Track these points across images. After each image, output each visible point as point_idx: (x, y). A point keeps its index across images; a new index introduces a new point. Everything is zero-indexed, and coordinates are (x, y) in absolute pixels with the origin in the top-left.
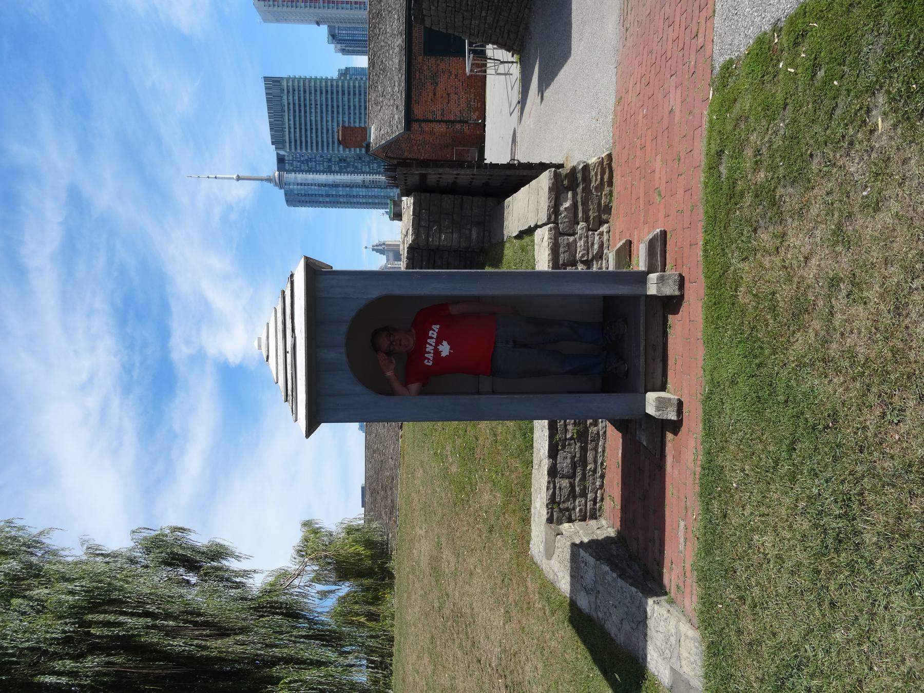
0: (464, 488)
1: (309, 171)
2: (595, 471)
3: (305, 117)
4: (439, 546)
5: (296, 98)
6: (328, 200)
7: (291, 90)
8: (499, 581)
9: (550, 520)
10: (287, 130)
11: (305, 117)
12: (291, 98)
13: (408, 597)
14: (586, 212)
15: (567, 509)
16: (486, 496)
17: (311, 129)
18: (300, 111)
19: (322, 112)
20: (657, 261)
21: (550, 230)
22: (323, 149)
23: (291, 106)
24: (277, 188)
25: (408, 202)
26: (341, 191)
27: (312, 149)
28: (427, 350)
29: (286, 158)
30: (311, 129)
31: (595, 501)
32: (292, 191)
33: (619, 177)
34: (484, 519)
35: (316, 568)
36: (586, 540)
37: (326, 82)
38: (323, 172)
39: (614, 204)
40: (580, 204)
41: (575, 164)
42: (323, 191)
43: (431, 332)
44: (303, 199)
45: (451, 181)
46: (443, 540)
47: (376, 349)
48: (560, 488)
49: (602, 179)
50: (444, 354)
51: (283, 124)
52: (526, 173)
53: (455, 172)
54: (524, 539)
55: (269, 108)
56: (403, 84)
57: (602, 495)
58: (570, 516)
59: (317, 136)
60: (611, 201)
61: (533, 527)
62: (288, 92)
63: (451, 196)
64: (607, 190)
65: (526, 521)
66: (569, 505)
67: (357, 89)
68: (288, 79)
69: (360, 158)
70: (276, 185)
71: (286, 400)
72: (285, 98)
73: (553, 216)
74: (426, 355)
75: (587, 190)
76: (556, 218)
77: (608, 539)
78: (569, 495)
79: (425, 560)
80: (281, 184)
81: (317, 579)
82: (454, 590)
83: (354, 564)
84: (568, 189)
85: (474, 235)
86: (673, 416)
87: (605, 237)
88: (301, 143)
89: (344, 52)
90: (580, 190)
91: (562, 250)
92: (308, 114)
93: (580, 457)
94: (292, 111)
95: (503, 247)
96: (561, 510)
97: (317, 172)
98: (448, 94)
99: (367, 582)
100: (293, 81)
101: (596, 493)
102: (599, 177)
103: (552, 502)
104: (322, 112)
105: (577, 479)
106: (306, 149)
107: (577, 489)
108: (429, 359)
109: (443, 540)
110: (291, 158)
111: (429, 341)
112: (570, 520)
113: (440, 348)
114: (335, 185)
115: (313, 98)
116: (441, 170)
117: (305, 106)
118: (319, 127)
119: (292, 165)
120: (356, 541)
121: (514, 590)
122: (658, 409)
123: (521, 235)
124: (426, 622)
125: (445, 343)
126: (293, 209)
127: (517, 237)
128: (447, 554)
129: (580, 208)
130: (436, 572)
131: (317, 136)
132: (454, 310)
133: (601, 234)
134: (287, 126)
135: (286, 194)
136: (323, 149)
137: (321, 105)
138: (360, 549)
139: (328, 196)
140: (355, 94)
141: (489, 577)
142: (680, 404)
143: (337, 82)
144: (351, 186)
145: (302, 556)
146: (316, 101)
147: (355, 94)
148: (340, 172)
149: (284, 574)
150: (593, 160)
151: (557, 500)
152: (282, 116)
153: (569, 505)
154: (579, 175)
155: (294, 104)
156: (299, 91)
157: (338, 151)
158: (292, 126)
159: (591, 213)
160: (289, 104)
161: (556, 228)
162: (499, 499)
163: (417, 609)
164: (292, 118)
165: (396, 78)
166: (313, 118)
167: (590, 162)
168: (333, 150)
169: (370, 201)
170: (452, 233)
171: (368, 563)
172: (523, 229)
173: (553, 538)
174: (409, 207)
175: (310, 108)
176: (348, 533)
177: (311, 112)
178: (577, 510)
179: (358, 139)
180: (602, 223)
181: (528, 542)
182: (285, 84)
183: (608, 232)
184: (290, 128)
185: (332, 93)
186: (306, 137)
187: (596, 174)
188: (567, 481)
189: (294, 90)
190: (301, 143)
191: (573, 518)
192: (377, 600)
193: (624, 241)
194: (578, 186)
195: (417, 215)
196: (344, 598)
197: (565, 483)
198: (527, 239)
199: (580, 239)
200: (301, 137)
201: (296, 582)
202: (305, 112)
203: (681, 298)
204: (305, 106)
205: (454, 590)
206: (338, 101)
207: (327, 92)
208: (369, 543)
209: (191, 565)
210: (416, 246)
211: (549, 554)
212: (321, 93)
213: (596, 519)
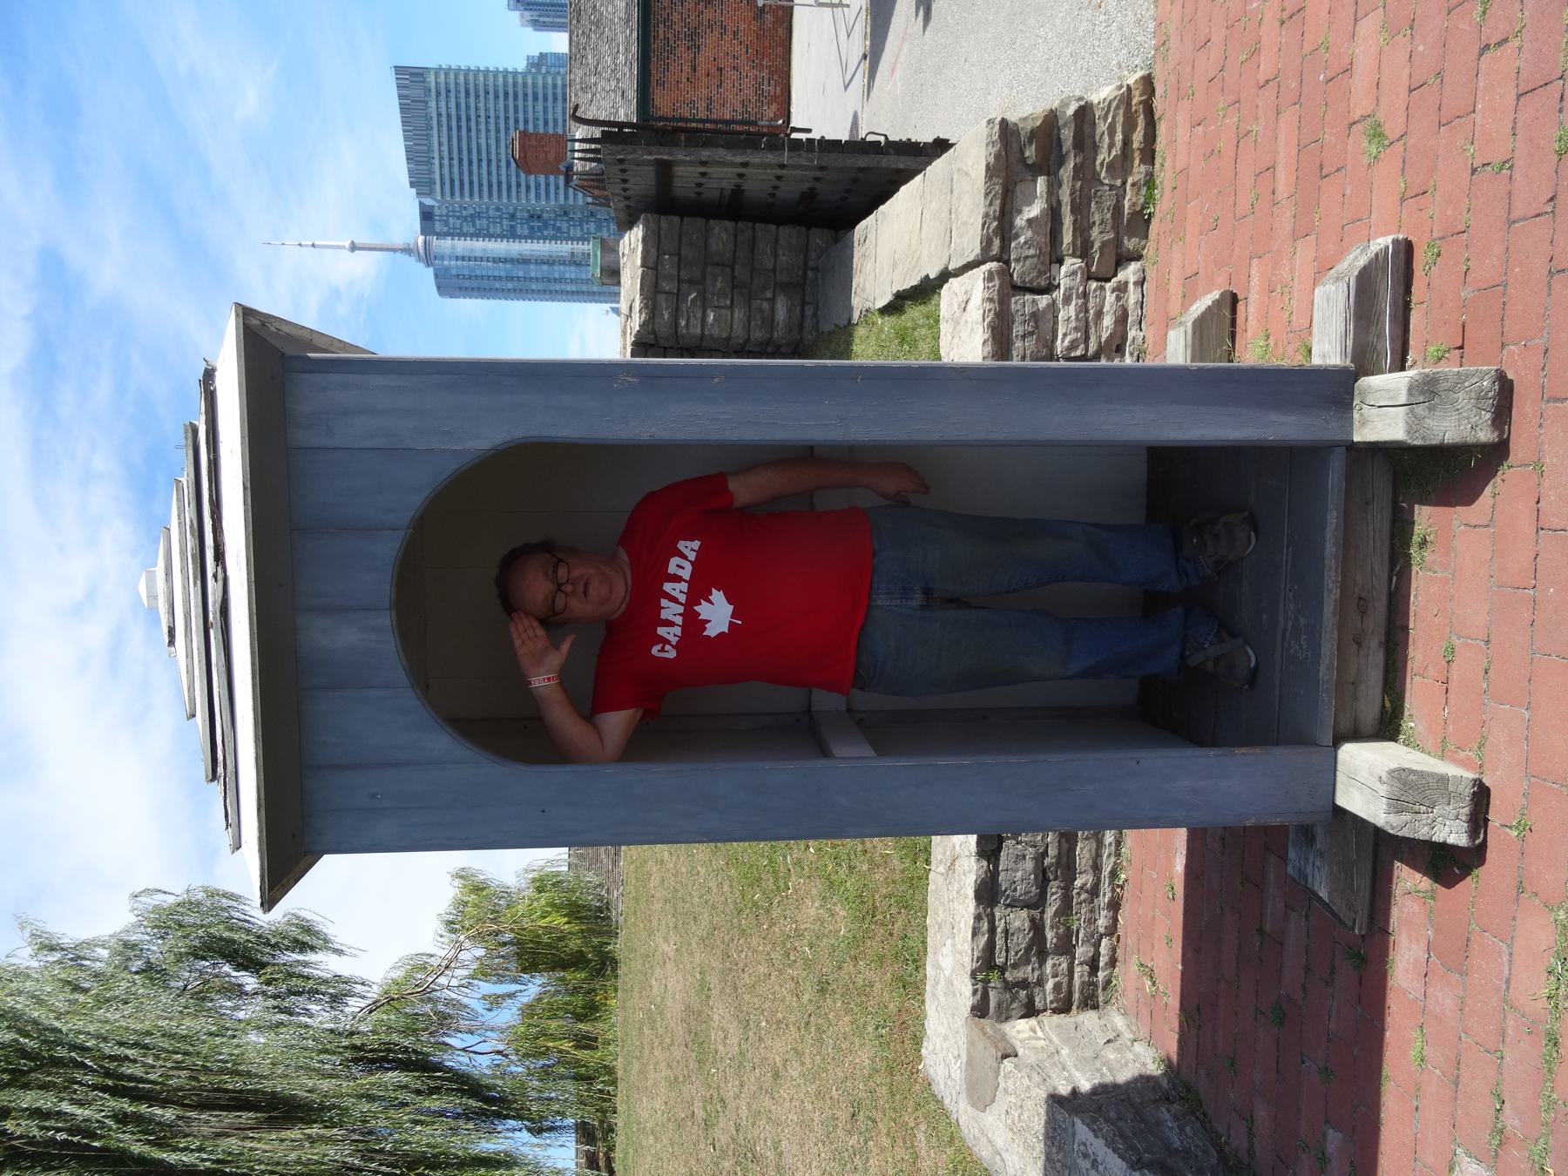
0: (759, 879)
1: (476, 235)
2: (1094, 891)
3: (469, 138)
4: (704, 989)
5: (453, 105)
6: (510, 285)
7: (443, 91)
8: (843, 1115)
9: (980, 1010)
10: (436, 161)
11: (469, 138)
12: (443, 104)
13: (640, 1072)
14: (1082, 229)
15: (1024, 984)
16: (811, 909)
17: (480, 160)
18: (459, 128)
19: (498, 131)
20: (1381, 335)
21: (990, 277)
22: (500, 196)
23: (444, 119)
24: (421, 265)
25: (632, 244)
26: (534, 271)
27: (481, 196)
28: (664, 615)
29: (437, 212)
30: (480, 160)
31: (1093, 965)
32: (447, 269)
33: (1182, 132)
34: (806, 960)
35: (481, 952)
36: (1085, 1086)
37: (505, 78)
38: (502, 236)
39: (1161, 210)
40: (1066, 210)
41: (1056, 104)
42: (502, 270)
43: (674, 561)
44: (467, 283)
45: (728, 185)
46: (714, 980)
47: (509, 606)
48: (1006, 931)
49: (1127, 142)
50: (712, 631)
51: (430, 150)
52: (902, 163)
53: (739, 159)
54: (905, 1032)
55: (404, 122)
56: (634, 49)
57: (1114, 950)
58: (1031, 999)
59: (489, 174)
60: (1150, 199)
61: (930, 1007)
62: (438, 94)
63: (729, 224)
64: (1139, 171)
65: (911, 984)
66: (1028, 972)
67: (559, 91)
68: (438, 71)
69: (566, 213)
70: (420, 259)
71: (214, 777)
72: (433, 104)
73: (997, 242)
74: (661, 631)
75: (1085, 173)
76: (1005, 247)
77: (1144, 1081)
78: (1028, 949)
79: (674, 1008)
80: (428, 257)
81: (484, 972)
82: (737, 1097)
83: (549, 946)
84: (1036, 169)
85: (781, 313)
86: (1453, 833)
87: (1132, 297)
88: (462, 184)
89: (537, 25)
90: (1066, 172)
91: (1018, 329)
92: (473, 133)
93: (1059, 857)
94: (445, 128)
95: (851, 335)
96: (1008, 986)
97: (490, 236)
98: (720, 70)
99: (576, 977)
100: (447, 75)
101: (1097, 945)
102: (1119, 137)
103: (987, 964)
104: (498, 131)
105: (1050, 912)
106: (471, 195)
107: (1049, 934)
108: (666, 641)
109: (714, 980)
110: (444, 212)
111: (668, 587)
112: (1030, 1011)
113: (703, 609)
114: (524, 261)
115: (481, 105)
116: (705, 154)
117: (469, 119)
118: (493, 157)
119: (446, 223)
120: (553, 905)
121: (883, 1149)
122: (1397, 804)
123: (896, 306)
124: (676, 1139)
125: (717, 596)
126: (448, 301)
127: (889, 310)
128: (720, 1013)
129: (1068, 221)
130: (698, 1040)
131: (489, 174)
132: (743, 490)
133: (1122, 288)
134: (436, 155)
135: (436, 276)
136: (500, 196)
137: (497, 118)
138: (559, 921)
139: (510, 278)
140: (555, 99)
141: (820, 1095)
142: (1481, 796)
143: (524, 78)
144: (549, 261)
145: (454, 931)
146: (487, 110)
147: (555, 99)
148: (531, 236)
149: (420, 965)
150: (1102, 94)
151: (1000, 961)
152: (429, 137)
153: (1028, 972)
154: (1067, 135)
155: (449, 116)
156: (457, 92)
157: (528, 199)
158: (446, 154)
159: (1095, 232)
160: (439, 115)
161: (1005, 273)
162: (843, 923)
163: (658, 1104)
164: (445, 140)
165: (621, 38)
166: (483, 141)
167: (1095, 98)
168: (518, 198)
169: (584, 288)
170: (731, 307)
171: (574, 944)
172: (906, 286)
173: (992, 1062)
174: (633, 251)
175: (477, 123)
176: (540, 890)
177: (478, 131)
178: (1049, 985)
179: (551, 157)
180: (1122, 260)
181: (918, 1041)
182: (431, 79)
183: (1141, 283)
184: (441, 158)
185: (516, 97)
186: (470, 174)
187: (1112, 130)
188: (1024, 913)
189: (448, 91)
190: (462, 184)
191: (1038, 1004)
192: (590, 1011)
193: (1216, 295)
194: (1061, 160)
195: (651, 266)
196: (530, 1006)
197: (1019, 919)
198: (914, 313)
199: (1067, 300)
200: (461, 174)
201: (443, 980)
202: (469, 130)
203: (1494, 455)
204: (469, 119)
205: (737, 1097)
206: (525, 112)
207: (506, 94)
208: (575, 911)
209: (245, 959)
210: (651, 339)
211: (982, 1095)
212: (496, 97)
213: (1095, 1007)
